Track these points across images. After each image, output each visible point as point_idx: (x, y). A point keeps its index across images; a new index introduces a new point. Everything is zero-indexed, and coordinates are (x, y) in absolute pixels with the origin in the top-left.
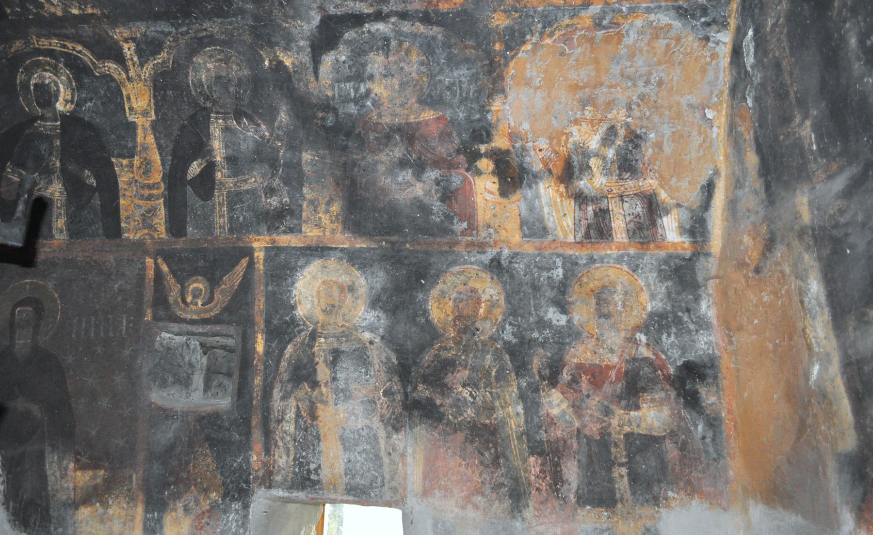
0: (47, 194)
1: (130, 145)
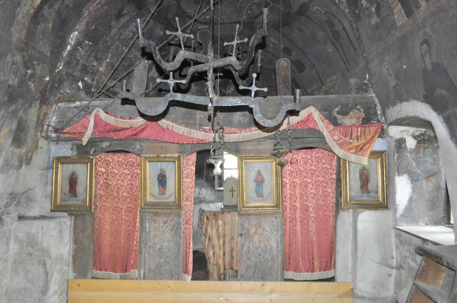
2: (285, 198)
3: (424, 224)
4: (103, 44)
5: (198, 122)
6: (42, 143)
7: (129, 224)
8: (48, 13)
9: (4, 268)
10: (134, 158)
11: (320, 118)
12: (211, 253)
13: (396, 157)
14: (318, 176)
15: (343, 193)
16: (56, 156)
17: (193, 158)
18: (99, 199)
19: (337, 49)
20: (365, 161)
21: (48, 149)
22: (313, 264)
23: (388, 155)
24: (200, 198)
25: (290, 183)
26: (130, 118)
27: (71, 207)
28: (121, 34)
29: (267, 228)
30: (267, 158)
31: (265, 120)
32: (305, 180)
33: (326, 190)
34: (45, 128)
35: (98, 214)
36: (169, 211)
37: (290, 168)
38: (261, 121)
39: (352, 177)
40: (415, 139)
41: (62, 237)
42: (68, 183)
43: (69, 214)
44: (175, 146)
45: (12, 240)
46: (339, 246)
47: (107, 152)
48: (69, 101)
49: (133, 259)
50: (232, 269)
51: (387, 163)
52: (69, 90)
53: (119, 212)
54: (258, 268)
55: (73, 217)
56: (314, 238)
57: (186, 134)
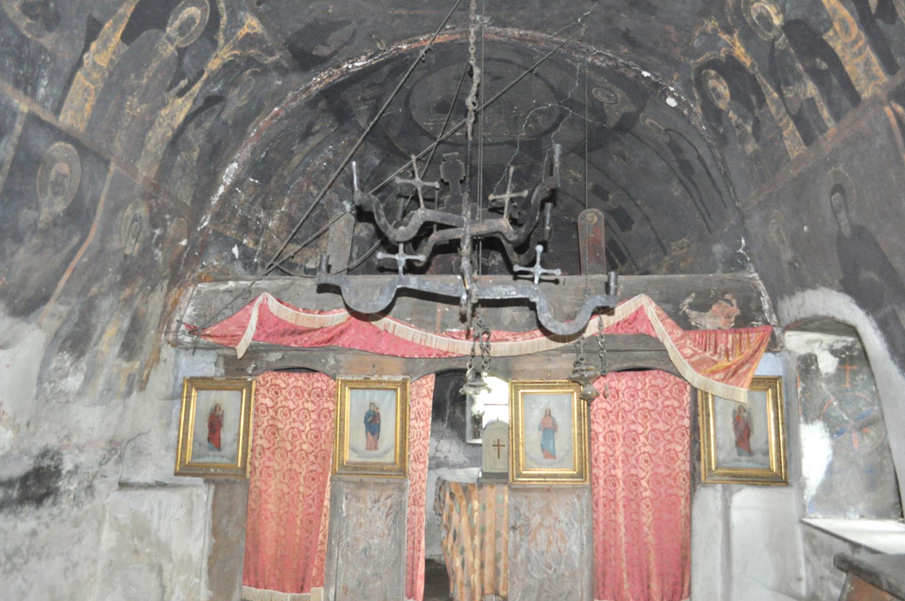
0: (809, 96)
1: (825, 16)
2: (596, 460)
3: (858, 516)
4: (276, 182)
5: (438, 320)
6: (167, 352)
7: (310, 501)
8: (193, 136)
9: (90, 576)
10: (323, 381)
11: (659, 315)
12: (458, 563)
13: (800, 389)
14: (657, 421)
15: (702, 454)
16: (189, 375)
17: (429, 383)
18: (260, 454)
19: (690, 193)
20: (742, 394)
21: (176, 362)
22: (649, 587)
23: (786, 385)
24: (439, 458)
25: (604, 433)
26: (321, 312)
27: (210, 467)
28: (308, 165)
29: (562, 516)
30: (562, 386)
31: (557, 323)
32: (633, 427)
33: (673, 446)
34: (174, 326)
35: (256, 482)
36: (384, 480)
37: (604, 405)
38: (550, 324)
39: (719, 423)
40: (836, 356)
41: (192, 522)
42: (206, 424)
43: (207, 481)
44: (396, 363)
45: (106, 525)
46: (698, 555)
47: (276, 370)
48: (216, 280)
49: (317, 567)
50: (496, 593)
51: (784, 400)
52: (217, 261)
53: (293, 479)
54: (546, 591)
55: (213, 487)
56: (650, 538)
57: (417, 341)
